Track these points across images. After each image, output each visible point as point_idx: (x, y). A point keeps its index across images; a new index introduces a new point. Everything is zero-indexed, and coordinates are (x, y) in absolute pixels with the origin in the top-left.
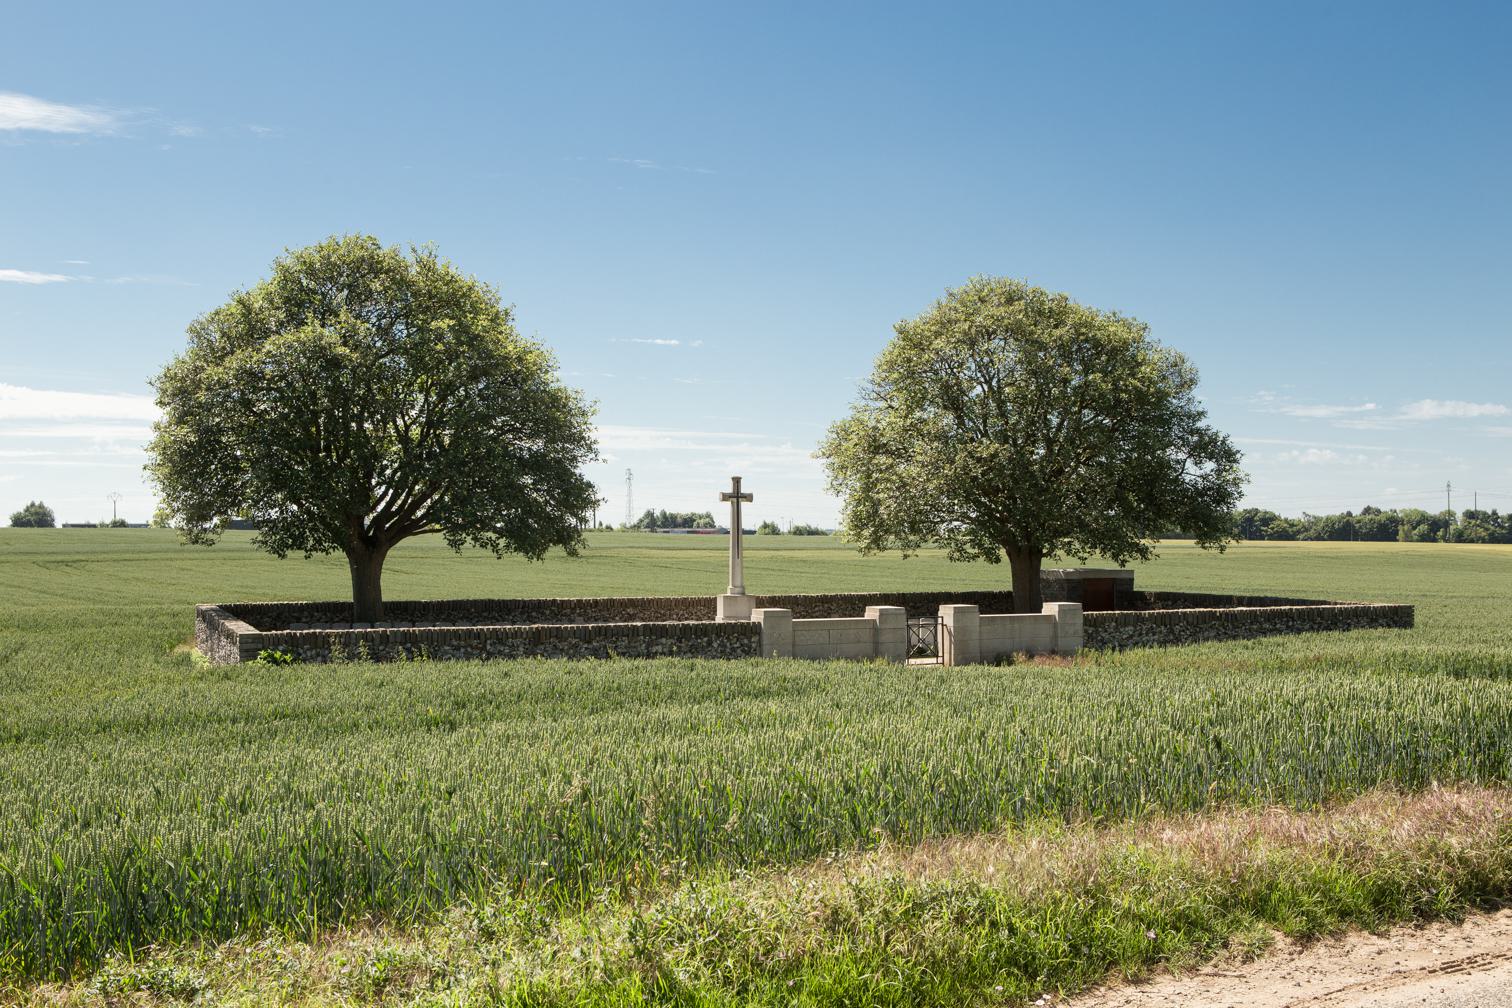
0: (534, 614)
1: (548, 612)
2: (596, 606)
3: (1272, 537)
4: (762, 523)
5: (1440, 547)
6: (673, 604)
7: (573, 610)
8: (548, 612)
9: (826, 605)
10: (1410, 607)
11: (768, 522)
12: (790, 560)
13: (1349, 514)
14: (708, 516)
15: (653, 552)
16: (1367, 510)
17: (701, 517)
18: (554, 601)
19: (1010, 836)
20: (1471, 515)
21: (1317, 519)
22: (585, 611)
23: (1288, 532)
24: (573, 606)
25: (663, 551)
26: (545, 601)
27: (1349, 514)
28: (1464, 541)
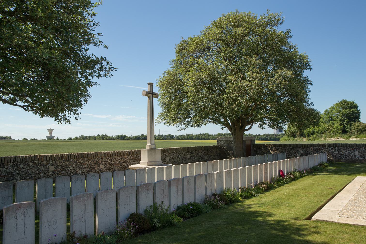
0: (22, 166)
1: (31, 164)
2: (62, 159)
3: (126, 139)
4: (23, 138)
5: (78, 140)
6: (103, 156)
7: (48, 161)
8: (31, 164)
9: (164, 154)
10: (67, 226)
11: (25, 138)
12: (44, 144)
13: (139, 135)
14: (10, 137)
15: (6, 143)
16: (142, 135)
17: (8, 137)
18: (36, 156)
19: (165, 122)
20: (159, 135)
21: (134, 136)
22: (55, 162)
23: (129, 138)
24: (48, 159)
25: (60, 142)
26: (29, 157)
27: (139, 135)
28: (199, 140)
